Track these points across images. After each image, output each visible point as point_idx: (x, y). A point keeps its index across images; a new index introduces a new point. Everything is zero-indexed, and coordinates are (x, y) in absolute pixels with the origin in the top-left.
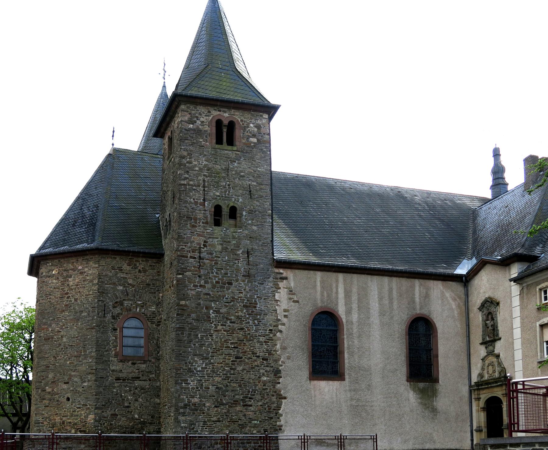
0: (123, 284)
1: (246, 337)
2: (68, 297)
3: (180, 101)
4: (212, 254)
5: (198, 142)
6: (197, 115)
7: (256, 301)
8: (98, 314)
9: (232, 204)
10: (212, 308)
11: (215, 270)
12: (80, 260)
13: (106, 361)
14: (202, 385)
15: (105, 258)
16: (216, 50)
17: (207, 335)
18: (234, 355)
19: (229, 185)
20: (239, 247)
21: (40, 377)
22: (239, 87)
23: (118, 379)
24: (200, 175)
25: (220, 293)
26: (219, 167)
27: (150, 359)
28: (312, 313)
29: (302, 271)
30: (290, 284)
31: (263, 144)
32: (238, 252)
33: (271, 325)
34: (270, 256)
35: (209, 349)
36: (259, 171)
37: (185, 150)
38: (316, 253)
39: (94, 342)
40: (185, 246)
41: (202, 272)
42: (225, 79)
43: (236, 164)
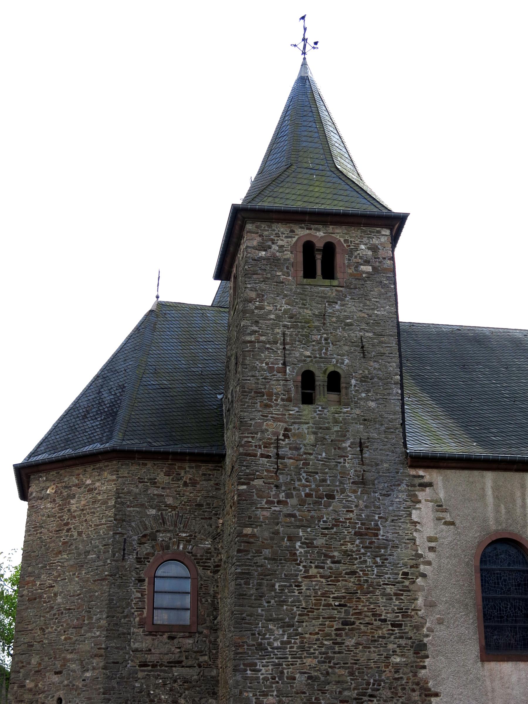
0: (157, 506)
1: (360, 586)
2: (68, 530)
3: (244, 218)
4: (297, 449)
5: (274, 276)
6: (272, 237)
7: (377, 525)
8: (114, 555)
9: (331, 369)
10: (299, 539)
11: (304, 475)
12: (89, 469)
13: (124, 634)
14: (282, 673)
15: (128, 465)
16: (305, 144)
17: (291, 586)
18: (340, 618)
19: (326, 339)
20: (345, 436)
21: (17, 663)
22: (342, 192)
23: (144, 665)
24: (277, 325)
25: (313, 513)
26: (310, 312)
27: (200, 629)
28: (480, 543)
29: (458, 471)
30: (437, 494)
31: (385, 277)
32: (344, 445)
33: (405, 565)
34: (400, 449)
35: (295, 609)
36: (377, 315)
37: (252, 289)
38: (482, 442)
39: (104, 603)
40: (253, 437)
41: (282, 479)
42: (318, 183)
43: (337, 307)
